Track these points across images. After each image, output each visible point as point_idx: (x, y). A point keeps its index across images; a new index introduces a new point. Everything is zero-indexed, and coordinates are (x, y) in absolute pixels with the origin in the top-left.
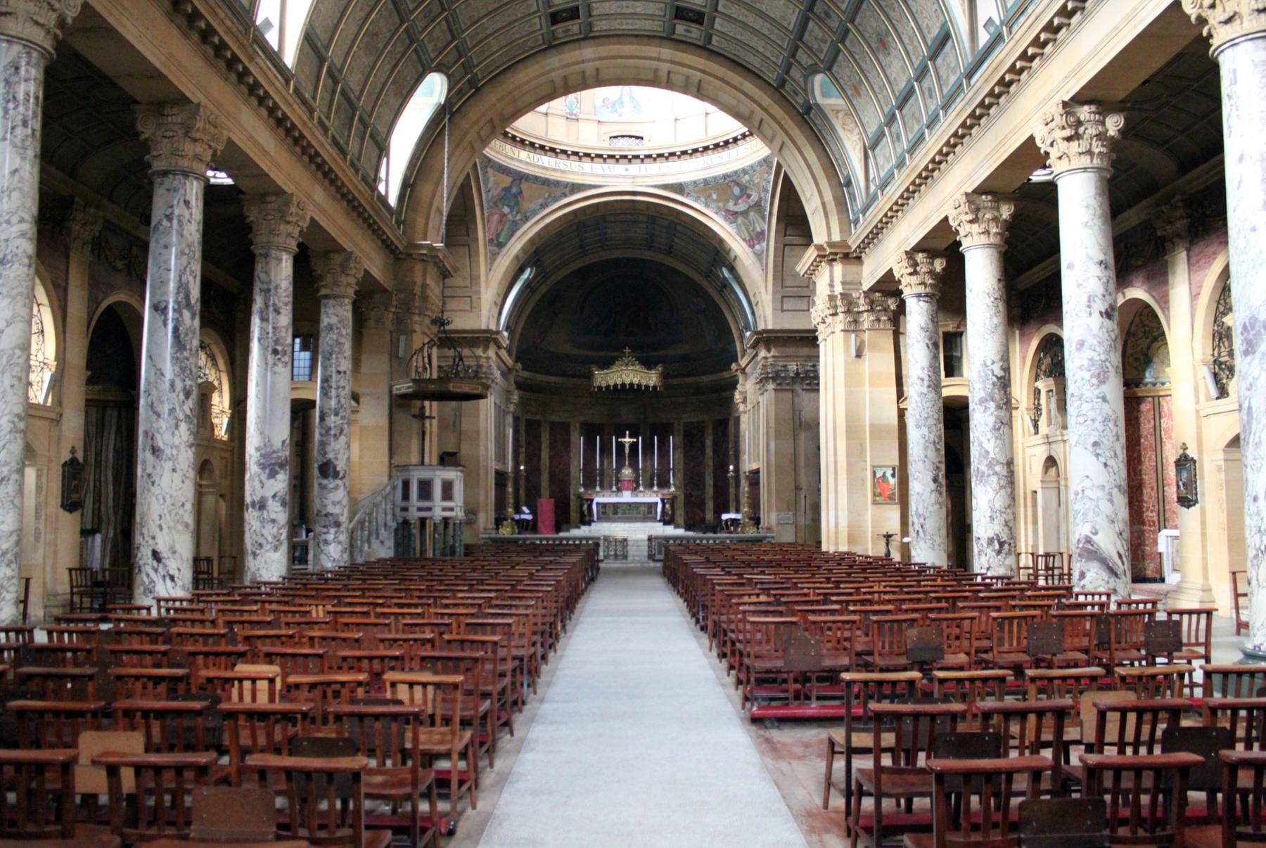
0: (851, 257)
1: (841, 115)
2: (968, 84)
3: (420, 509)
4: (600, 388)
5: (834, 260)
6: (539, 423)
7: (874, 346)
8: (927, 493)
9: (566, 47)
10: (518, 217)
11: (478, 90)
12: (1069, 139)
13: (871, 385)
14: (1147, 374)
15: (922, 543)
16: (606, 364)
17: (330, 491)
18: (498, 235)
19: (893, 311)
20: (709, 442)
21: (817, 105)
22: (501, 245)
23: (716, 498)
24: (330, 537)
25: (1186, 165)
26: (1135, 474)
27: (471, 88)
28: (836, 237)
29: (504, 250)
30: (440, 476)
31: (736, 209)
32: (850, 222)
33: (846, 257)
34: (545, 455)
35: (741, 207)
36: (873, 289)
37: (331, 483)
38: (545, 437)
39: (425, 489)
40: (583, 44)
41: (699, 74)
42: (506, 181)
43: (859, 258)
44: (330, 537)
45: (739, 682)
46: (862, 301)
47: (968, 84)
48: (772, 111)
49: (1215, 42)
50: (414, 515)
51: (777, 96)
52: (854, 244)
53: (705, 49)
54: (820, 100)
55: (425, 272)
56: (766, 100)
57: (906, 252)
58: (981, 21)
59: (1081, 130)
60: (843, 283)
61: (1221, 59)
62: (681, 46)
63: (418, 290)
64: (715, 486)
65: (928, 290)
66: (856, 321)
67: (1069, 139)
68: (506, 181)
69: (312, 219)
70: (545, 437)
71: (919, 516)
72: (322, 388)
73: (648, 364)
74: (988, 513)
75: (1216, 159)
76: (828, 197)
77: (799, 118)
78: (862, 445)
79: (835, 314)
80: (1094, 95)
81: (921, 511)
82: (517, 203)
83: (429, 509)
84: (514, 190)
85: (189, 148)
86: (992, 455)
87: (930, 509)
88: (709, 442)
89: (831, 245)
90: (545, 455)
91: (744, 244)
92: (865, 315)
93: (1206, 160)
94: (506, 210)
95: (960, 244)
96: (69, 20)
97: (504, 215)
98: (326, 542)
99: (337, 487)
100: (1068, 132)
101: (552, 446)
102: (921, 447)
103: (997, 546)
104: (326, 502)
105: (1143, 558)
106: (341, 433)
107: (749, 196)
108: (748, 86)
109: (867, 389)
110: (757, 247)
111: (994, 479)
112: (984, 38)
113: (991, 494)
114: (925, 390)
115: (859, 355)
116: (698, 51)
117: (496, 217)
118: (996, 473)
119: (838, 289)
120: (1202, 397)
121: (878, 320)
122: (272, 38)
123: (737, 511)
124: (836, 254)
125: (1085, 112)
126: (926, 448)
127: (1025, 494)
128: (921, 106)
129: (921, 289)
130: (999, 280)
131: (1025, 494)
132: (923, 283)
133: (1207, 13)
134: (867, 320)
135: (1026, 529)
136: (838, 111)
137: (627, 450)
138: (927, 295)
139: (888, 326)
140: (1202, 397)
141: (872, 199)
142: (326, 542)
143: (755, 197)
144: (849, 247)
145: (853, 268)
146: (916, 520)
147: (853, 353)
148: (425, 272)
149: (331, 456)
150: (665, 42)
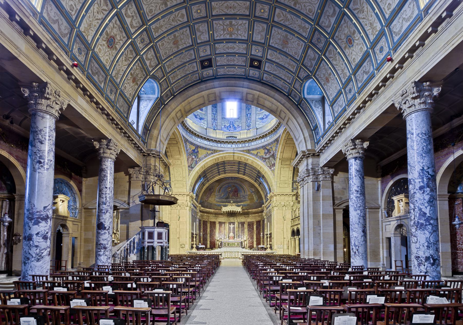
0: (316, 155)
1: (314, 102)
2: (336, 123)
3: (148, 243)
4: (224, 212)
5: (309, 157)
6: (207, 221)
7: (324, 187)
8: (360, 237)
9: (208, 82)
10: (198, 160)
11: (175, 96)
12: (352, 149)
13: (323, 200)
14: (459, 189)
15: (357, 257)
16: (225, 206)
17: (102, 235)
18: (191, 165)
19: (332, 174)
20: (255, 227)
21: (305, 98)
22: (192, 168)
23: (257, 241)
24: (102, 253)
25: (398, 150)
26: (453, 230)
27: (172, 95)
28: (309, 147)
29: (193, 169)
30: (157, 231)
31: (266, 157)
32: (312, 130)
33: (314, 155)
34: (208, 230)
35: (268, 156)
36: (324, 166)
37: (103, 232)
38: (209, 225)
39: (151, 235)
40: (214, 80)
41: (258, 93)
42: (193, 148)
43: (318, 155)
44: (102, 253)
45: (250, 273)
46: (320, 171)
47: (336, 123)
48: (286, 105)
49: (348, 158)
50: (146, 244)
51: (288, 99)
52: (317, 149)
53: (260, 81)
54: (306, 96)
55: (155, 161)
56: (284, 100)
57: (415, 82)
58: (327, 121)
59: (356, 147)
60: (312, 165)
61: (408, 119)
62: (252, 81)
63: (152, 167)
64: (257, 238)
65: (361, 155)
66: (317, 178)
67: (352, 149)
68: (193, 148)
69: (121, 150)
70: (209, 225)
71: (356, 246)
72: (99, 194)
73: (237, 202)
74: (426, 244)
75: (405, 149)
76: (307, 135)
77: (296, 107)
78: (319, 222)
79: (309, 176)
80: (361, 137)
81: (357, 244)
82: (197, 155)
83: (152, 242)
84: (196, 151)
85: (108, 151)
86: (428, 215)
87: (361, 243)
88: (255, 227)
89: (308, 150)
90: (208, 230)
91: (268, 168)
92: (321, 175)
93: (402, 149)
94: (194, 157)
95: (346, 158)
96: (64, 109)
97: (193, 159)
98: (99, 255)
99: (105, 233)
100: (353, 147)
101: (211, 227)
102: (357, 218)
103: (432, 261)
104: (100, 239)
105: (457, 264)
106: (107, 212)
107: (270, 153)
108: (277, 96)
109: (321, 202)
110: (272, 168)
111: (430, 227)
112: (327, 126)
113: (428, 235)
114: (359, 195)
115: (318, 189)
116: (258, 83)
117: (190, 159)
118: (430, 224)
119: (310, 167)
120: (384, 217)
121: (326, 177)
122: (135, 126)
123: (263, 245)
124: (310, 154)
125: (357, 141)
126: (359, 219)
127: (383, 239)
128: (354, 87)
129: (357, 155)
130: (431, 127)
131: (383, 239)
132: (358, 152)
133: (346, 153)
134: (321, 177)
135: (383, 251)
136: (313, 100)
137: (232, 229)
138: (360, 157)
139: (330, 179)
140: (384, 217)
141: (326, 132)
142: (99, 255)
143: (272, 153)
144: (316, 151)
145: (316, 159)
146: (354, 247)
147: (316, 189)
148: (155, 161)
149: (102, 221)
150: (246, 80)
